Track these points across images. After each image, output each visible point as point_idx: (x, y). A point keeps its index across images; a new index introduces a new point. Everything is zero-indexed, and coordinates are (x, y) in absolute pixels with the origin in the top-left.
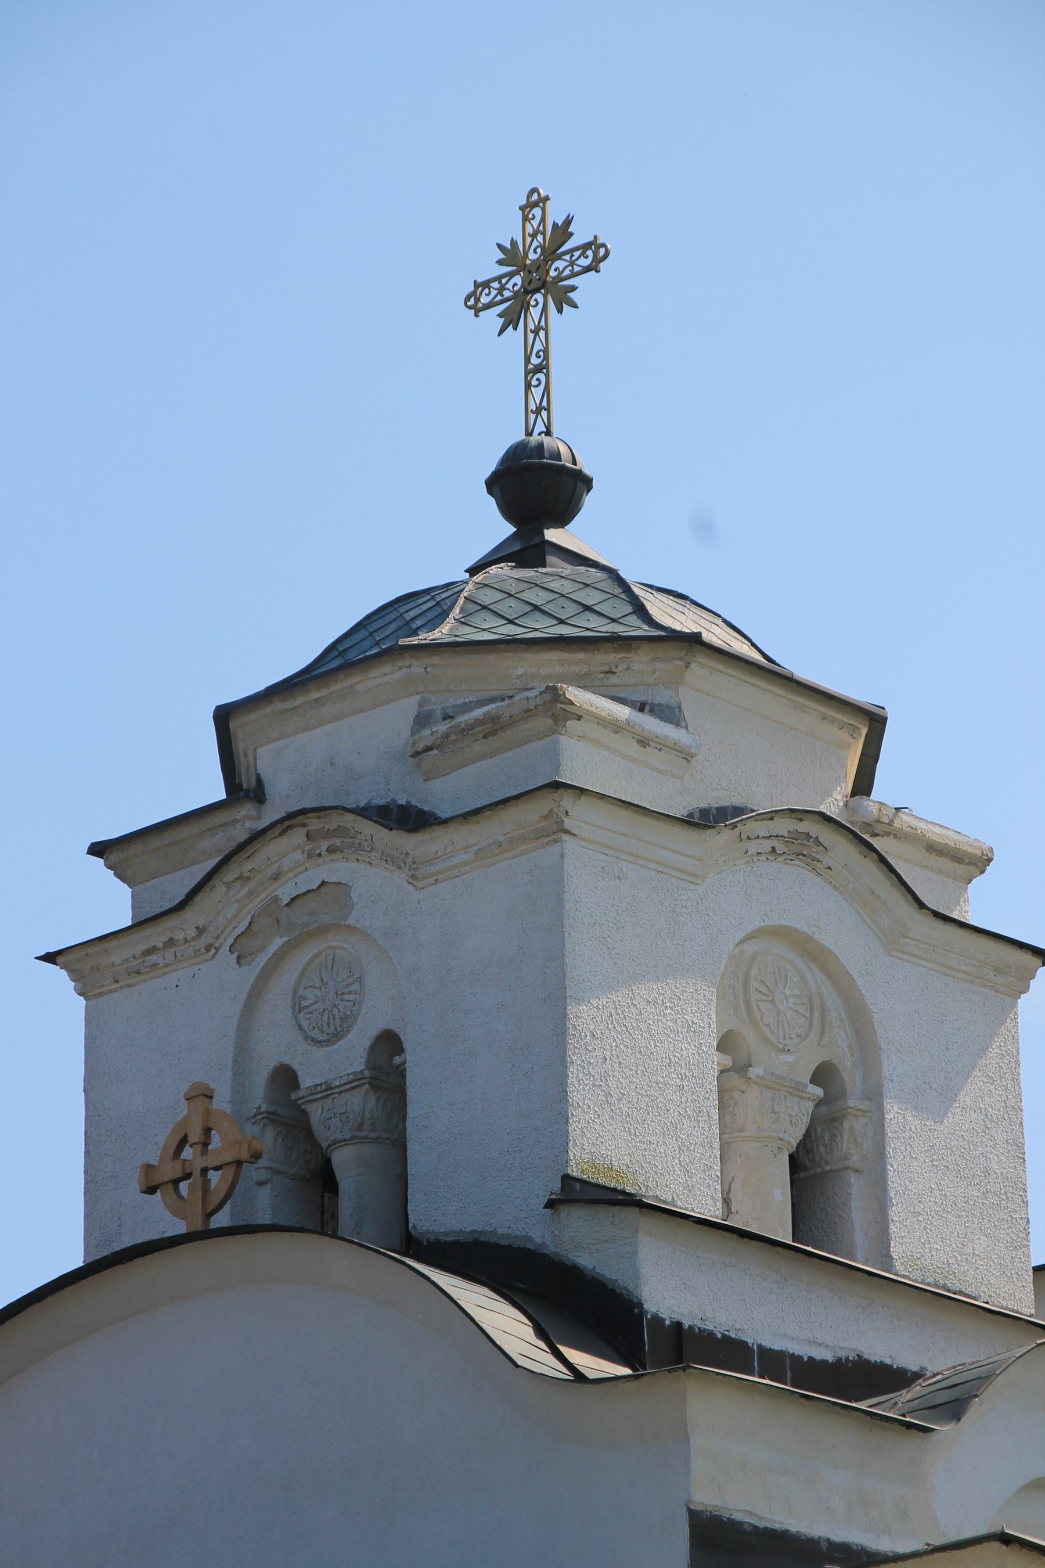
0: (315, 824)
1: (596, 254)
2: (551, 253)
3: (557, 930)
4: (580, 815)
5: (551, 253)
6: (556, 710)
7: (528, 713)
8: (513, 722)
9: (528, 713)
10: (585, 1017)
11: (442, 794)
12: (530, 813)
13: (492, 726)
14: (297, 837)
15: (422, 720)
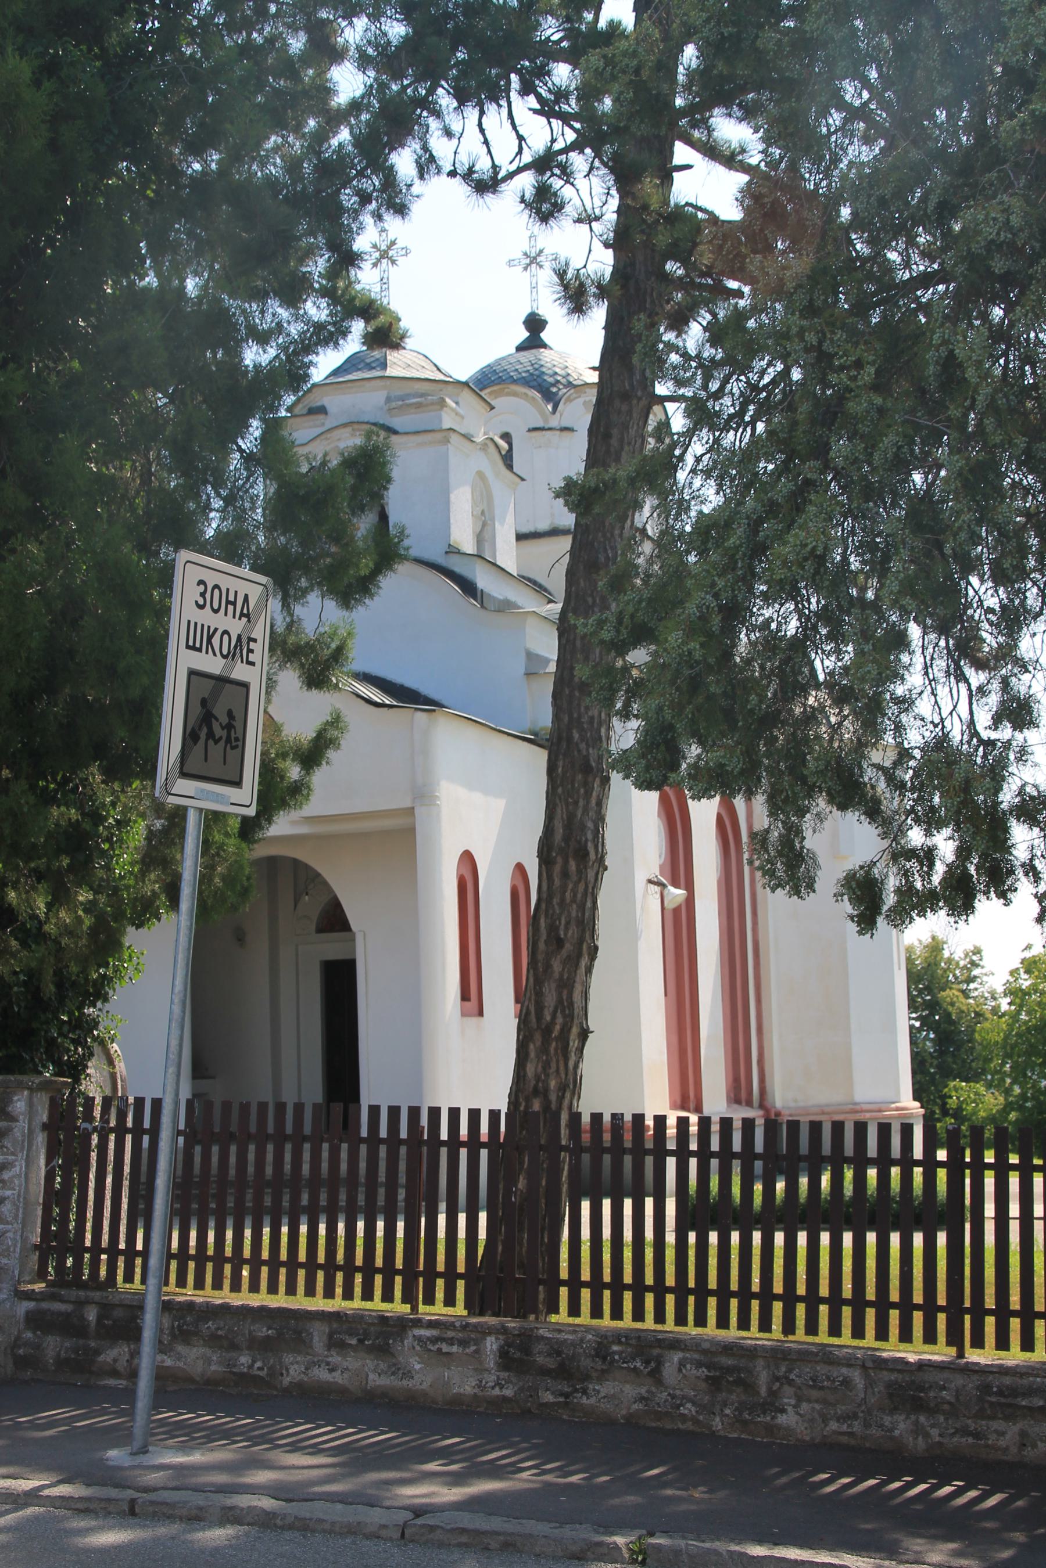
0: (356, 426)
1: (407, 251)
2: (389, 248)
3: (446, 470)
4: (454, 438)
5: (389, 248)
6: (442, 403)
7: (432, 404)
8: (427, 405)
9: (432, 404)
10: (452, 497)
11: (396, 422)
12: (438, 436)
13: (419, 406)
14: (349, 429)
15: (388, 400)
